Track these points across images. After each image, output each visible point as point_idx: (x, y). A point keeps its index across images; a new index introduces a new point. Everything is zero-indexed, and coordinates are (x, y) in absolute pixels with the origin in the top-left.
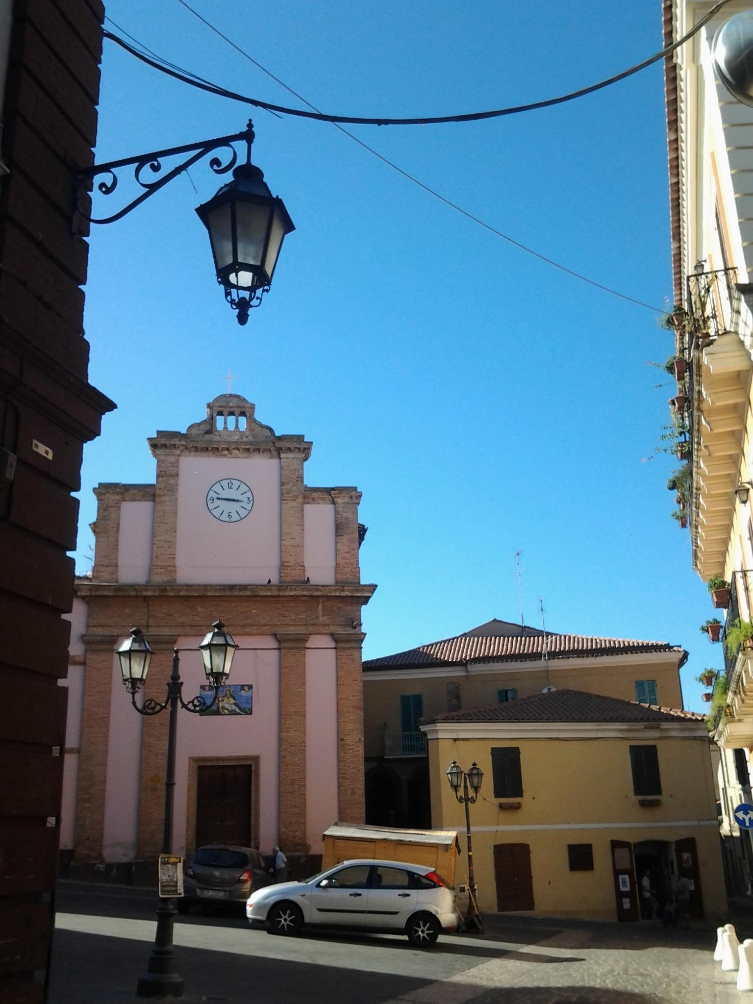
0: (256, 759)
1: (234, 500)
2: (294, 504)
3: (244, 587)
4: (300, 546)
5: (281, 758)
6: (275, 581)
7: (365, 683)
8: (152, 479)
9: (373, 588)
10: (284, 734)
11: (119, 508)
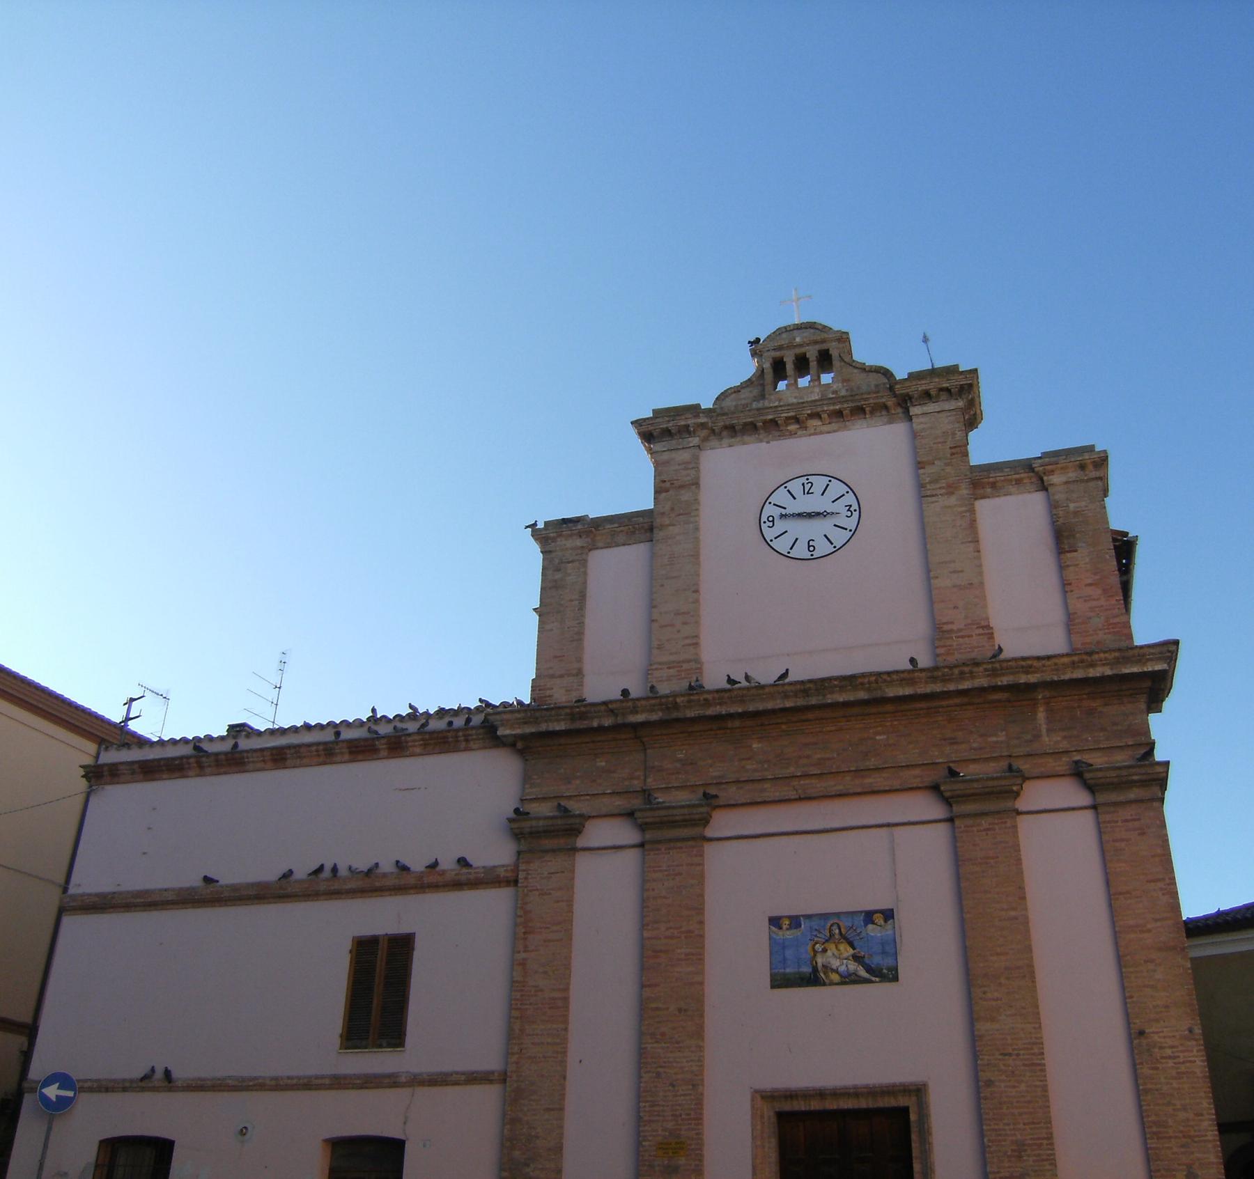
0: (918, 1091)
1: (818, 514)
2: (953, 500)
3: (850, 681)
4: (975, 586)
5: (981, 1087)
6: (924, 661)
7: (1198, 964)
8: (645, 501)
9: (1169, 650)
10: (982, 1027)
11: (584, 563)
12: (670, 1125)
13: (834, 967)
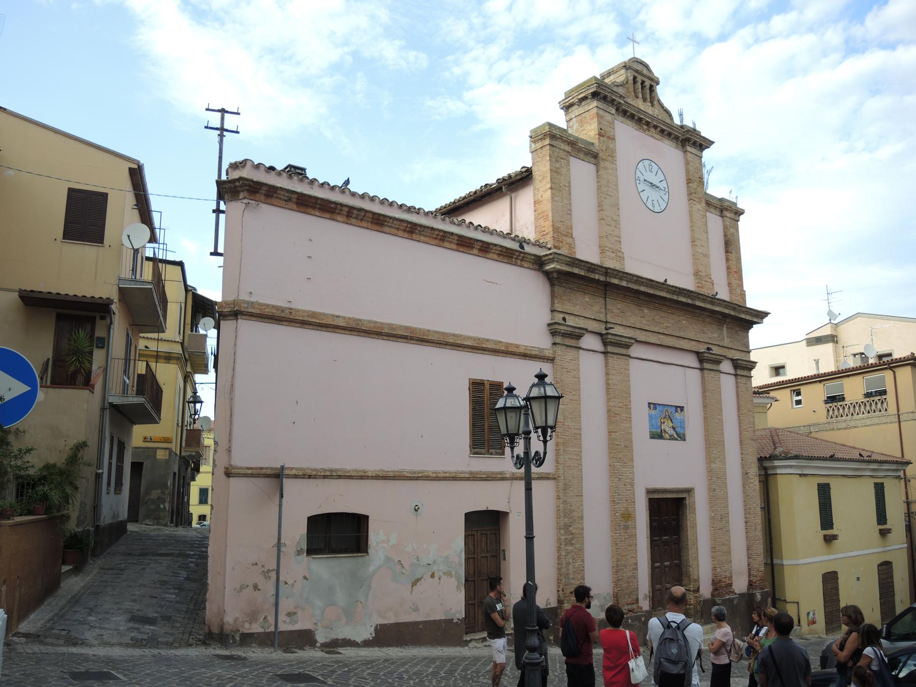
0: (689, 491)
12: (625, 505)
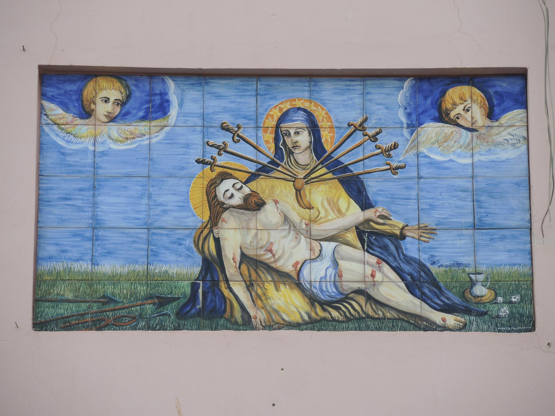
13: (286, 265)
